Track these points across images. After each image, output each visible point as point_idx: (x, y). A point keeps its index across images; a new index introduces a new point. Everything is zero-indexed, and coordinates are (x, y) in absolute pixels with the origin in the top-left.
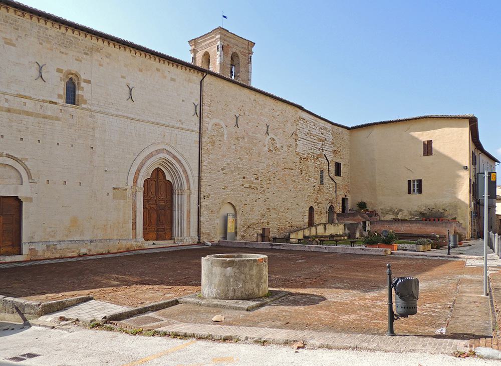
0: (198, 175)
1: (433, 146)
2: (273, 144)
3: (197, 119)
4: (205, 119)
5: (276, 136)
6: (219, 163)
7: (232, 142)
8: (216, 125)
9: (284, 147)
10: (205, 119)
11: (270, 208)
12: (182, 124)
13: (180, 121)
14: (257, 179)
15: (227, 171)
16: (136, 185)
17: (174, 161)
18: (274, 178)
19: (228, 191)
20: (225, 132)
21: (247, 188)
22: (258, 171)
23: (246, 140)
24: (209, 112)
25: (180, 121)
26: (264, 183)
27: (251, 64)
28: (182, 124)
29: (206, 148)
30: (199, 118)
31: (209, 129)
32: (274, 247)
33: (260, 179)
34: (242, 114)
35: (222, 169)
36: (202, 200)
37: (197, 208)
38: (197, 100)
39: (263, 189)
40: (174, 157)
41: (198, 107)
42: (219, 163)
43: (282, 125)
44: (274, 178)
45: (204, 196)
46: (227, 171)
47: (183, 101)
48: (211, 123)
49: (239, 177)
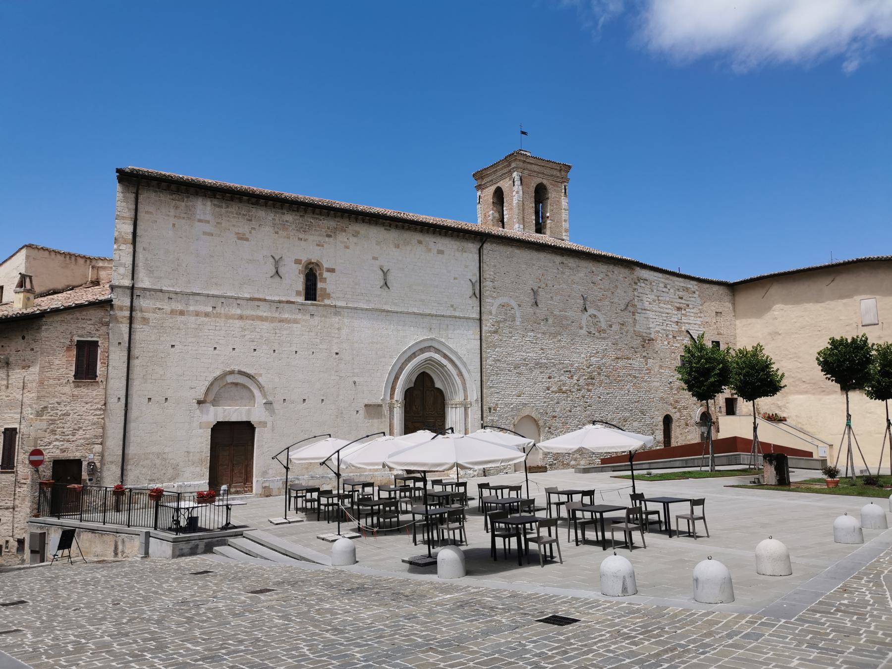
2: (595, 324)
9: (613, 326)
12: (455, 310)
13: (452, 306)
20: (518, 314)
23: (550, 321)
25: (452, 306)
34: (544, 286)
45: (490, 409)
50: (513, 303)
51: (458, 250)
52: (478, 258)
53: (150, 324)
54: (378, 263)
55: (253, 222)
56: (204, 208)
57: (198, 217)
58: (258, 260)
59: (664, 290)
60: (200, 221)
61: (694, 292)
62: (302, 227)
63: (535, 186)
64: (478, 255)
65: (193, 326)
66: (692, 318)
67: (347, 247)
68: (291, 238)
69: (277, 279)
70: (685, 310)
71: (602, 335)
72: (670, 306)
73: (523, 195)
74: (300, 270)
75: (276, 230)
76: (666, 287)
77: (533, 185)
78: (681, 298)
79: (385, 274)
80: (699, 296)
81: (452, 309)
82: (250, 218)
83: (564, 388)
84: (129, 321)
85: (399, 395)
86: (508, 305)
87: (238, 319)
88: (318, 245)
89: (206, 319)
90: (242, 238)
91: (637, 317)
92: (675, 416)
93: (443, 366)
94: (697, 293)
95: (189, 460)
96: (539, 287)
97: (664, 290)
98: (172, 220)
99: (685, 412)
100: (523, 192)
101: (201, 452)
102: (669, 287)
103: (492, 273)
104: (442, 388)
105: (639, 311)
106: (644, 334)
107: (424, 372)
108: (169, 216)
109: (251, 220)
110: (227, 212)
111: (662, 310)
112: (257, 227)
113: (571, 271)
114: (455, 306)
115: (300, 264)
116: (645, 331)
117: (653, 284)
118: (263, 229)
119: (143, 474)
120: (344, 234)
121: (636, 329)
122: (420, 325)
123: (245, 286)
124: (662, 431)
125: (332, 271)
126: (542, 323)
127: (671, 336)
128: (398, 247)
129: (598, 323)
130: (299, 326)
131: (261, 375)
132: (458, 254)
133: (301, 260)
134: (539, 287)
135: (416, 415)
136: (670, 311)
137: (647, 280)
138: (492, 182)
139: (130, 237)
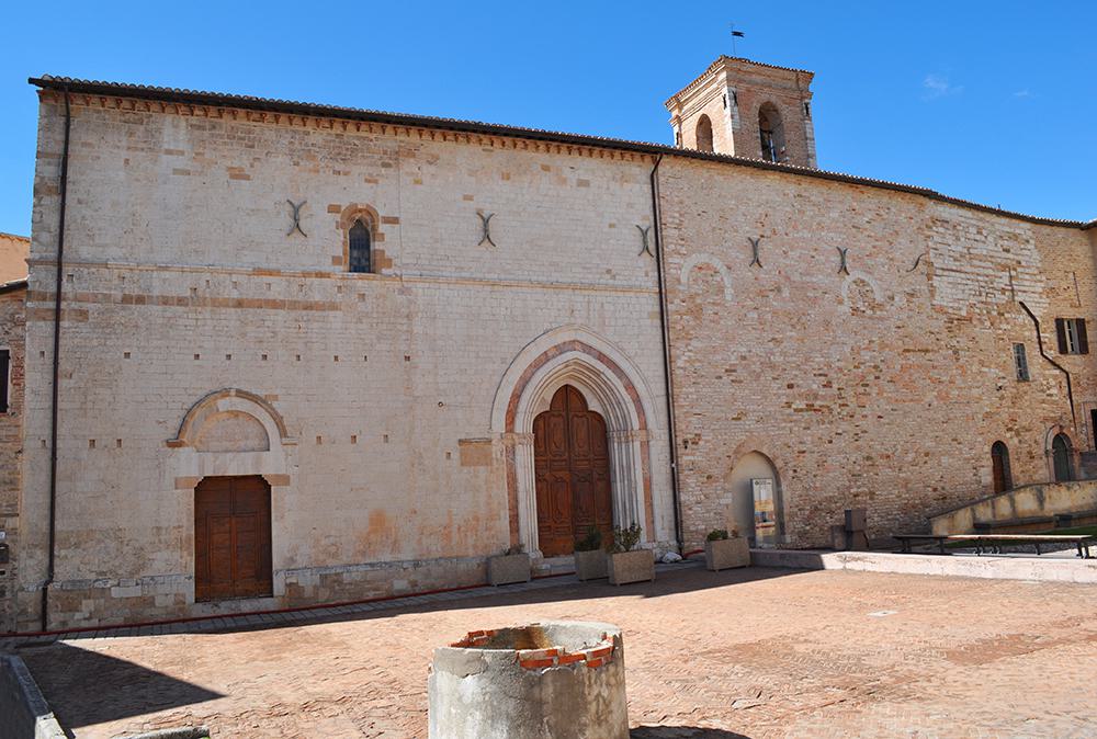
0: (663, 392)
2: (863, 295)
3: (648, 262)
4: (670, 260)
9: (896, 299)
11: (873, 455)
12: (614, 277)
13: (609, 271)
14: (828, 385)
19: (749, 423)
20: (727, 282)
23: (786, 293)
25: (609, 271)
26: (849, 393)
28: (614, 277)
29: (679, 327)
31: (684, 280)
32: (849, 566)
33: (835, 386)
34: (768, 233)
36: (681, 451)
37: (669, 471)
40: (601, 357)
41: (651, 234)
42: (718, 357)
44: (877, 378)
45: (686, 442)
46: (741, 374)
49: (775, 385)
50: (717, 263)
51: (614, 178)
52: (651, 192)
53: (90, 320)
54: (472, 205)
55: (256, 149)
56: (174, 129)
57: (166, 146)
58: (266, 210)
59: (978, 237)
60: (169, 152)
61: (1028, 241)
62: (339, 154)
63: (758, 106)
64: (650, 186)
65: (160, 321)
66: (1027, 283)
67: (418, 182)
68: (322, 170)
69: (297, 238)
70: (1015, 269)
71: (878, 313)
72: (990, 265)
73: (740, 119)
74: (337, 222)
75: (295, 159)
76: (979, 233)
77: (756, 106)
78: (1007, 251)
79: (486, 222)
80: (1036, 247)
81: (608, 276)
82: (250, 143)
83: (818, 403)
84: (54, 317)
85: (524, 424)
86: (708, 267)
87: (234, 307)
88: (367, 181)
89: (181, 309)
90: (238, 175)
91: (936, 281)
92: (1012, 443)
93: (598, 374)
94: (1031, 241)
95: (160, 541)
96: (762, 236)
97: (978, 237)
98: (124, 154)
99: (1027, 436)
100: (741, 117)
101: (179, 527)
102: (985, 232)
103: (677, 215)
104: (600, 411)
105: (939, 272)
106: (950, 311)
107: (567, 385)
108: (118, 147)
109: (253, 147)
110: (212, 135)
111: (976, 270)
112: (263, 157)
113: (816, 209)
114: (614, 272)
115: (338, 212)
116: (951, 305)
117: (958, 227)
118: (274, 159)
119: (85, 564)
120: (412, 160)
121: (935, 302)
122: (552, 305)
123: (246, 253)
124: (991, 469)
125: (395, 221)
126: (771, 296)
127: (995, 313)
128: (508, 179)
129: (869, 294)
130: (338, 313)
131: (276, 398)
132: (614, 186)
133: (340, 206)
134: (762, 236)
135: (557, 458)
136: (991, 272)
137: (947, 222)
138: (694, 110)
139: (57, 184)
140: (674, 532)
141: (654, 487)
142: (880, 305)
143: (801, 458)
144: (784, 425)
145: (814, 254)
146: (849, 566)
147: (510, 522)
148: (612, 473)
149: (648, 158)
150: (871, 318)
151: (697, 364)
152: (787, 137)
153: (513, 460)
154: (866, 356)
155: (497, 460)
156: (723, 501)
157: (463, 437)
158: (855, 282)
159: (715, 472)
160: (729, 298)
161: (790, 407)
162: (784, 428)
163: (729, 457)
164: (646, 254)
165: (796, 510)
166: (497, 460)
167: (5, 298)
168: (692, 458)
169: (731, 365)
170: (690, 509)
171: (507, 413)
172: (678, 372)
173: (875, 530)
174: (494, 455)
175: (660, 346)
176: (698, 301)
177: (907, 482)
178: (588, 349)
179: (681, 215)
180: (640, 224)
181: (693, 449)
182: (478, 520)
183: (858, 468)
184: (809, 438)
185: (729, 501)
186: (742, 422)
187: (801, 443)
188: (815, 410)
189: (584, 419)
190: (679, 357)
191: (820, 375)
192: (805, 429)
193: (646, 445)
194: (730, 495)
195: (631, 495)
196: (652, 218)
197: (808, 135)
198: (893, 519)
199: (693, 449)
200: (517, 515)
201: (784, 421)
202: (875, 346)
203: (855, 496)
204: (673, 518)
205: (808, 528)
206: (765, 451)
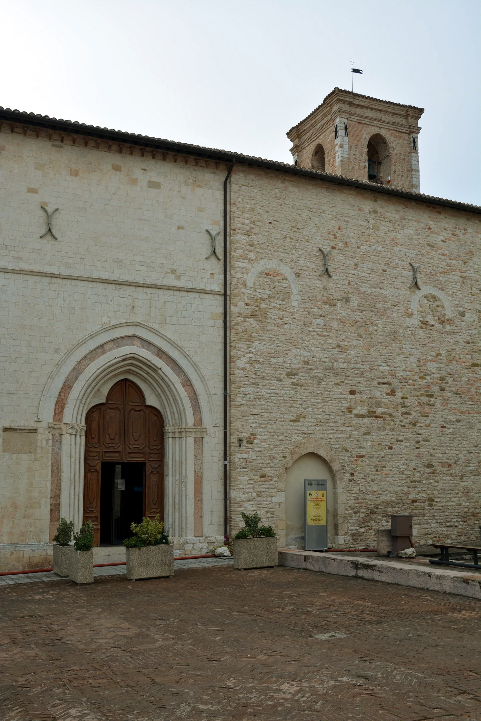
0: (221, 391)
1: (292, 146)
2: (434, 310)
3: (217, 267)
4: (238, 264)
5: (442, 289)
6: (281, 360)
7: (315, 309)
8: (267, 274)
9: (468, 315)
10: (238, 264)
11: (434, 463)
12: (178, 277)
13: (173, 272)
14: (392, 393)
15: (302, 377)
16: (60, 420)
17: (158, 362)
18: (443, 389)
19: (307, 425)
20: (295, 289)
21: (363, 416)
22: (393, 374)
23: (354, 302)
24: (248, 247)
25: (173, 272)
26: (412, 402)
27: (417, 153)
28: (178, 277)
29: (241, 329)
30: (222, 263)
31: (250, 283)
32: (361, 573)
33: (399, 394)
34: (341, 245)
35: (288, 374)
36: (234, 449)
37: (222, 468)
38: (215, 223)
39: (410, 417)
40: (161, 353)
41: (220, 239)
42: (281, 360)
43: (459, 264)
44: (443, 389)
45: (240, 440)
46: (302, 377)
47: (180, 228)
48: (252, 270)
49: (336, 390)
50: (286, 270)
52: (223, 198)
63: (368, 138)
64: (223, 193)
79: (49, 217)
83: (379, 411)
86: (277, 273)
96: (334, 248)
134: (334, 248)
140: (222, 528)
141: (205, 482)
142: (451, 322)
143: (359, 462)
144: (343, 428)
145: (385, 268)
146: (361, 573)
147: (51, 511)
148: (166, 468)
149: (222, 166)
150: (439, 332)
151: (258, 366)
152: (394, 168)
153: (60, 449)
154: (432, 367)
155: (42, 448)
156: (275, 500)
157: (7, 425)
158: (426, 297)
159: (269, 471)
160: (295, 303)
161: (351, 412)
162: (343, 432)
163: (285, 457)
164: (214, 260)
165: (350, 511)
166: (42, 448)
167: (480, 362)
168: (245, 456)
169: (292, 368)
170: (241, 506)
171: (57, 403)
172: (237, 372)
173: (432, 536)
174: (39, 444)
175: (221, 346)
176: (263, 305)
177: (467, 492)
178: (147, 344)
179: (252, 222)
180: (209, 228)
181: (248, 448)
182: (16, 508)
183: (418, 474)
184: (369, 443)
185: (282, 500)
186: (300, 424)
187: (360, 447)
188: (376, 417)
189: (142, 413)
190: (238, 358)
191: (384, 383)
192: (365, 434)
193: (199, 441)
194: (283, 494)
195: (180, 490)
196: (222, 223)
197: (413, 168)
198: (452, 526)
199: (248, 448)
200: (59, 504)
201: (344, 425)
202: (443, 359)
203: (414, 501)
204: (222, 514)
205: (362, 530)
206: (322, 453)
